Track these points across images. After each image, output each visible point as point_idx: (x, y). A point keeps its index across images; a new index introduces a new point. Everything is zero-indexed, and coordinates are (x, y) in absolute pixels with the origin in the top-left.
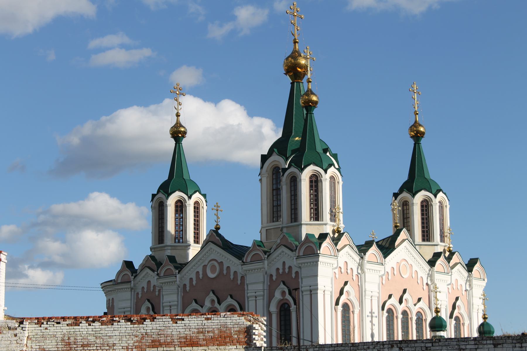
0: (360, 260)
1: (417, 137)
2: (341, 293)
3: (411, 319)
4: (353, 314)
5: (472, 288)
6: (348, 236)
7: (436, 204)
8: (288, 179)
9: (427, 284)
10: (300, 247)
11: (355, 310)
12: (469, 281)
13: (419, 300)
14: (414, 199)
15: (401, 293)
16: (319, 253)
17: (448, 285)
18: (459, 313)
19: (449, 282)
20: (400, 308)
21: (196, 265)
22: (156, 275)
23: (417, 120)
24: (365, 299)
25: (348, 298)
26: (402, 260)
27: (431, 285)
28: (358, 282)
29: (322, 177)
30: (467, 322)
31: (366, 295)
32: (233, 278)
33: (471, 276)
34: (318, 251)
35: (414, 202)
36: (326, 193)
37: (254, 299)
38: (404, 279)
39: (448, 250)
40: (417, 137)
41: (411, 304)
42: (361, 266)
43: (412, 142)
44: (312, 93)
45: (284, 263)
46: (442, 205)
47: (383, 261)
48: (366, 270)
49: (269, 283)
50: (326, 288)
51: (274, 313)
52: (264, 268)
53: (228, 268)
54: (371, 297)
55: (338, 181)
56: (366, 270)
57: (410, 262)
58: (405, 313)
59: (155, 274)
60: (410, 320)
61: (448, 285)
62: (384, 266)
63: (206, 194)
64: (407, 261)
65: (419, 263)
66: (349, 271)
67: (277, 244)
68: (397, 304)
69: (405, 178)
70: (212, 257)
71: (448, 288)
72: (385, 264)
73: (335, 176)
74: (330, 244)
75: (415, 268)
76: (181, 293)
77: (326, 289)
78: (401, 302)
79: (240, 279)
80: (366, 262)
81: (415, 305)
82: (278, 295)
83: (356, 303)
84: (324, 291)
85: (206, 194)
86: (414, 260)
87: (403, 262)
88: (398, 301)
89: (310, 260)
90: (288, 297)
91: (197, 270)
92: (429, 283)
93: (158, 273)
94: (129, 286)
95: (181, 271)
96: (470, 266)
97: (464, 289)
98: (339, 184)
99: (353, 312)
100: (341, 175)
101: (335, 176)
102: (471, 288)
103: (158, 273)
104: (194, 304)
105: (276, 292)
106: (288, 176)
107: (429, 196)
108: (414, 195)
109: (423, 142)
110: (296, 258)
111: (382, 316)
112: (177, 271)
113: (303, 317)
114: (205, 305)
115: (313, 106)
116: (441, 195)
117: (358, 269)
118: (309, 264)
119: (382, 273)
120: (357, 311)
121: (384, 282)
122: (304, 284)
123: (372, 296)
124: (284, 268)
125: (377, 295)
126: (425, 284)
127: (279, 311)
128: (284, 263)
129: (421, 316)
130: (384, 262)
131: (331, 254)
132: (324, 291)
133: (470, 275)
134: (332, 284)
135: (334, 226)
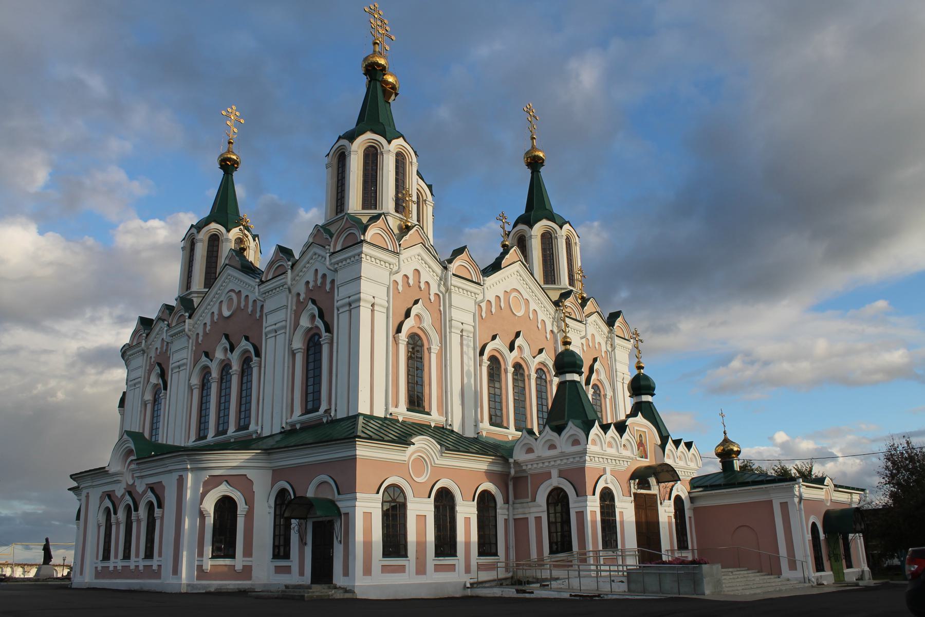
0: (442, 273)
1: (535, 164)
2: (408, 314)
3: (529, 376)
4: (430, 353)
5: (615, 349)
6: (421, 233)
7: (562, 236)
8: (335, 156)
9: (552, 331)
10: (337, 235)
11: (432, 347)
12: (610, 338)
13: (541, 351)
14: (532, 230)
15: (513, 338)
16: (362, 239)
17: (582, 338)
18: (598, 380)
19: (583, 334)
20: (511, 358)
21: (214, 299)
22: (166, 326)
23: (535, 144)
24: (450, 332)
25: (420, 326)
26: (512, 289)
27: (558, 333)
28: (440, 306)
29: (383, 148)
30: (609, 394)
31: (451, 326)
32: (252, 311)
33: (613, 331)
34: (362, 236)
35: (532, 233)
36: (388, 171)
37: (347, 308)
38: (517, 317)
39: (580, 297)
40: (535, 164)
41: (527, 354)
42: (443, 280)
43: (529, 172)
44: (396, 96)
45: (316, 270)
46: (569, 241)
47: (480, 279)
48: (452, 287)
49: (294, 308)
50: (377, 301)
51: (298, 352)
52: (286, 283)
53: (247, 296)
54: (462, 331)
55: (410, 160)
56: (452, 287)
57: (526, 296)
58: (518, 367)
59: (165, 324)
60: (526, 378)
61: (582, 338)
62: (483, 287)
63: (431, 185)
64: (521, 294)
65: (539, 299)
66: (423, 286)
67: (308, 245)
68: (506, 351)
69: (522, 211)
70: (231, 286)
71: (582, 344)
72: (484, 284)
73: (405, 152)
74: (385, 231)
75: (533, 306)
76: (192, 347)
77: (376, 302)
78: (512, 348)
79: (259, 309)
80: (450, 273)
81: (534, 357)
82: (305, 322)
83: (435, 337)
84: (373, 305)
85: (431, 185)
86: (531, 294)
87: (514, 293)
88: (508, 347)
89: (346, 256)
90: (319, 323)
91: (212, 311)
92: (556, 331)
93: (168, 322)
94: (140, 348)
95: (193, 315)
96: (611, 320)
97: (604, 349)
98: (411, 164)
99: (429, 349)
100: (432, 194)
101: (405, 152)
102: (613, 348)
103: (170, 322)
104: (204, 358)
105: (301, 317)
106: (335, 154)
107: (556, 229)
108: (531, 226)
109: (543, 171)
110: (329, 256)
111: (480, 365)
112: (187, 314)
113: (337, 351)
114: (216, 356)
115: (380, 70)
116: (567, 226)
117: (439, 286)
118: (352, 259)
119: (480, 298)
120: (435, 348)
121: (484, 315)
122: (341, 295)
123: (462, 330)
124: (315, 281)
125: (472, 329)
126: (548, 331)
127: (306, 349)
128: (316, 270)
129: (544, 375)
130: (482, 282)
131: (472, 278)
132: (373, 305)
133: (612, 330)
134: (388, 296)
135: (401, 220)
